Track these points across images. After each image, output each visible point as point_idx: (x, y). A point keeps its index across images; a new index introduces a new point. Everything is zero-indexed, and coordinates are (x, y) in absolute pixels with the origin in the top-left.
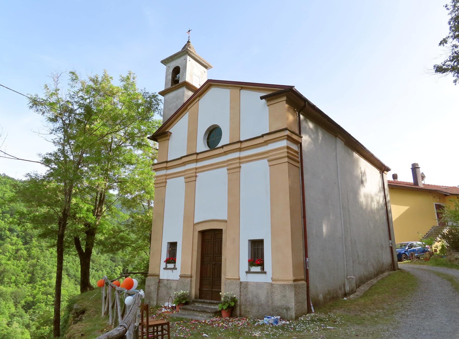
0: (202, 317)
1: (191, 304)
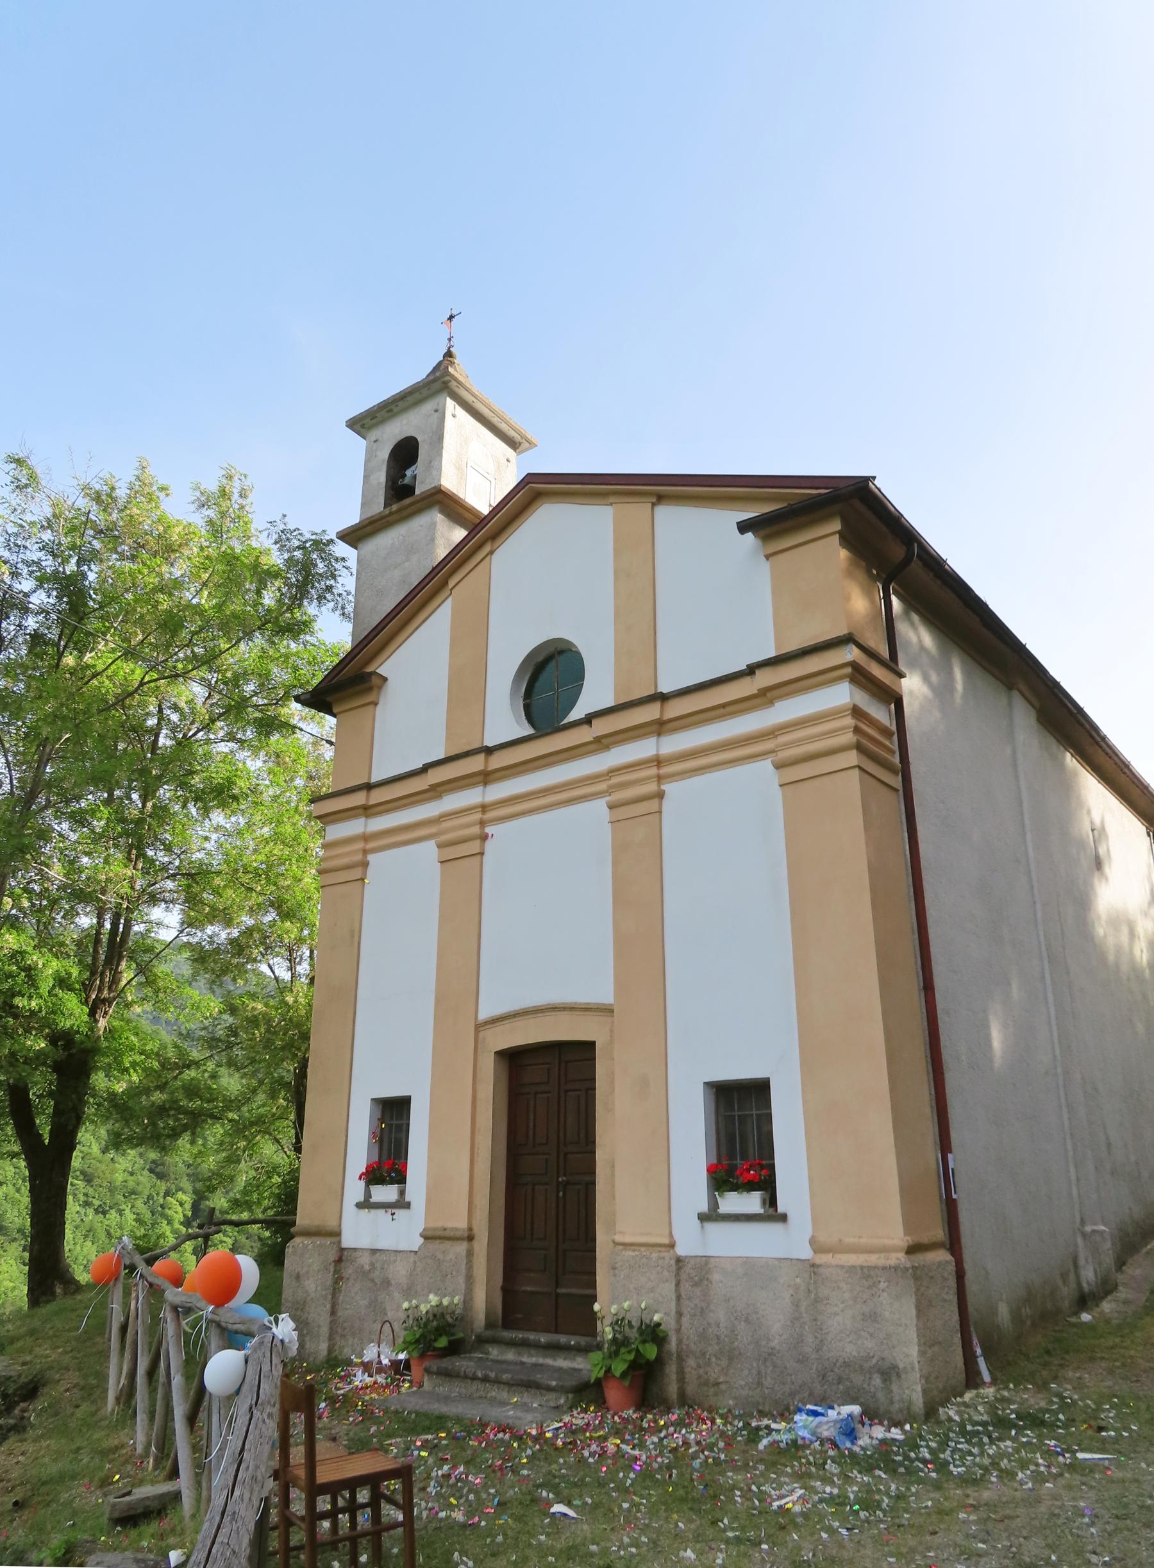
0: (526, 1407)
1: (470, 1352)
